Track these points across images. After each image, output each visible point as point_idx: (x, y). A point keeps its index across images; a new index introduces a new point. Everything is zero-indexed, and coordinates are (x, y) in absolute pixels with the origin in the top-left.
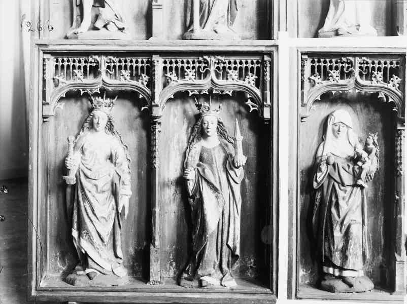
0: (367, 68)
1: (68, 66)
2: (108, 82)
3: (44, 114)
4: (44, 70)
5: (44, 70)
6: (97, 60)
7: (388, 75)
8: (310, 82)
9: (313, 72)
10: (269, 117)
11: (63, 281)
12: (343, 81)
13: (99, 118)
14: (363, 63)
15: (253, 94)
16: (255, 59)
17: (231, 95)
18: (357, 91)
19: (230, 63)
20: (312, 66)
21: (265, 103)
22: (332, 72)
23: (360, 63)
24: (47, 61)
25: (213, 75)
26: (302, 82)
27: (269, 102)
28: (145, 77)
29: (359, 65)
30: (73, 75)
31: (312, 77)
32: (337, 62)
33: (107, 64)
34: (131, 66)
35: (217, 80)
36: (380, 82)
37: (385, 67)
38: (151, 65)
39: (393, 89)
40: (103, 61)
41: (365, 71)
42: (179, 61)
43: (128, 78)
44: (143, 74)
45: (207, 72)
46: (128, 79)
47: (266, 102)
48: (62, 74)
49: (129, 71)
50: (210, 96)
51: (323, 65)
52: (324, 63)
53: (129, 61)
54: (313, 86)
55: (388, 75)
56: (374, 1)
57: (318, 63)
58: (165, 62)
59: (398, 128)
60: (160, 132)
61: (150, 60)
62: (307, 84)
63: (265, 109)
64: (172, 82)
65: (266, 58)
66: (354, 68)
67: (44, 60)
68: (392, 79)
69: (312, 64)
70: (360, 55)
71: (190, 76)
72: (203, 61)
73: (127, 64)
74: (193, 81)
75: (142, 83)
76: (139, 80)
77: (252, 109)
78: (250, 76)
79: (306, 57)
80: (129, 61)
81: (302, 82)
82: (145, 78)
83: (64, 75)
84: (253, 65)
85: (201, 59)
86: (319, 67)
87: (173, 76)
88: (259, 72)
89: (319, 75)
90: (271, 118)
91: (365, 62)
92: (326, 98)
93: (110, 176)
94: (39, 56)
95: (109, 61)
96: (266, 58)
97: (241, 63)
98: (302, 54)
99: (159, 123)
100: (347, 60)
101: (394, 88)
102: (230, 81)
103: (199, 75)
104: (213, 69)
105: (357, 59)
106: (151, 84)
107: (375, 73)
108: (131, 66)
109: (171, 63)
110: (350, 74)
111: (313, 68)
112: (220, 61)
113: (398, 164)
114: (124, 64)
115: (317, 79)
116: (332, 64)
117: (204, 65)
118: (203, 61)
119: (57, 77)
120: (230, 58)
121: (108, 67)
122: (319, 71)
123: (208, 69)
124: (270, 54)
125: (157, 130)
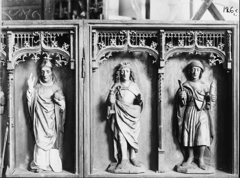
0: (135, 37)
1: (20, 39)
6: (124, 33)
7: (218, 42)
9: (100, 41)
10: (73, 68)
11: (175, 171)
12: (188, 46)
14: (132, 35)
17: (112, 55)
19: (181, 35)
23: (198, 36)
25: (129, 43)
26: (93, 47)
31: (100, 43)
33: (44, 37)
35: (198, 46)
36: (211, 46)
37: (205, 38)
38: (159, 35)
40: (128, 34)
41: (134, 40)
45: (125, 42)
46: (211, 45)
47: (229, 59)
50: (195, 56)
51: (106, 36)
52: (205, 36)
53: (22, 36)
54: (100, 49)
55: (218, 42)
56: (204, 1)
57: (145, 36)
58: (16, 36)
61: (6, 34)
62: (96, 47)
63: (71, 63)
64: (170, 49)
65: (229, 32)
67: (93, 33)
68: (219, 44)
69: (198, 37)
71: (113, 43)
72: (190, 34)
73: (28, 37)
74: (115, 46)
78: (221, 44)
79: (94, 31)
80: (22, 36)
81: (93, 47)
85: (121, 32)
86: (103, 38)
87: (103, 44)
88: (225, 40)
89: (104, 42)
90: (74, 69)
91: (133, 34)
92: (116, 55)
93: (52, 118)
95: (132, 34)
96: (229, 32)
98: (93, 29)
99: (163, 74)
100: (191, 34)
102: (53, 48)
104: (129, 38)
105: (129, 31)
106: (159, 48)
107: (112, 40)
109: (212, 35)
111: (100, 38)
113: (8, 90)
114: (26, 37)
115: (170, 45)
117: (123, 36)
118: (190, 34)
120: (167, 32)
121: (45, 39)
123: (126, 39)
124: (73, 29)
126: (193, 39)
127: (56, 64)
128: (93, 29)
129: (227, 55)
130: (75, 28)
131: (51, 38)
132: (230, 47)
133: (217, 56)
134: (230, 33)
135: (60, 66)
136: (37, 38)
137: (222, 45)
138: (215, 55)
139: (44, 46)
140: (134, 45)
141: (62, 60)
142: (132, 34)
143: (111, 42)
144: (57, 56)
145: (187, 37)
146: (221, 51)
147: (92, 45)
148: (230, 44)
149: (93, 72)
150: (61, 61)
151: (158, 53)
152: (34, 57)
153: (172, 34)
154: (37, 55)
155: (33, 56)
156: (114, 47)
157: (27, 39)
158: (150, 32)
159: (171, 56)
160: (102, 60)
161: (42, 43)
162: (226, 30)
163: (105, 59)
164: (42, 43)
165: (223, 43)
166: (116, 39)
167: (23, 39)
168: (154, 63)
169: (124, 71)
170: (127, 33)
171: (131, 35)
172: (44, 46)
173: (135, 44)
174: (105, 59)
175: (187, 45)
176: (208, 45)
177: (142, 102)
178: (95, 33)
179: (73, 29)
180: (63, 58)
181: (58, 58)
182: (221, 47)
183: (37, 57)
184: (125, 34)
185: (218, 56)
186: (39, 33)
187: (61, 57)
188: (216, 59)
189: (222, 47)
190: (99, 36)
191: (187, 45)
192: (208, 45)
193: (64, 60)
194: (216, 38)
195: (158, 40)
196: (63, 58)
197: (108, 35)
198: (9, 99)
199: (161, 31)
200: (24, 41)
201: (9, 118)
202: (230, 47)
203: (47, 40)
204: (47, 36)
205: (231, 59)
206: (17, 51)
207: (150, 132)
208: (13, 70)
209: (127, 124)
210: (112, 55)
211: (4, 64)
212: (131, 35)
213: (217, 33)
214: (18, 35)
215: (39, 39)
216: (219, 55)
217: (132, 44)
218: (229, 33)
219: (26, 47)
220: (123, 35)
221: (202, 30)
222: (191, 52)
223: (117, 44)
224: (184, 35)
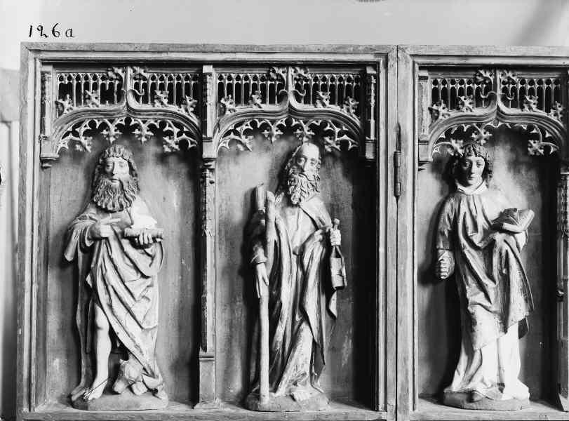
0: (514, 90)
2: (482, 114)
3: (44, 154)
4: (43, 89)
5: (43, 89)
6: (281, 76)
8: (57, 107)
13: (114, 163)
14: (508, 83)
15: (351, 126)
16: (190, 72)
17: (124, 124)
18: (500, 124)
19: (532, 83)
20: (219, 84)
21: (204, 136)
22: (462, 98)
23: (504, 83)
24: (47, 75)
27: (372, 137)
28: (190, 100)
29: (502, 86)
30: (85, 99)
31: (435, 107)
32: (103, 78)
34: (171, 86)
35: (507, 109)
38: (201, 79)
39: (554, 119)
42: (224, 77)
43: (165, 101)
44: (189, 95)
47: (369, 137)
48: (230, 96)
49: (168, 92)
53: (66, 78)
57: (452, 84)
59: (562, 173)
60: (212, 182)
65: (370, 71)
66: (287, 89)
67: (43, 74)
70: (132, 63)
75: (187, 110)
76: (182, 106)
77: (190, 146)
79: (49, 68)
82: (190, 101)
83: (232, 98)
84: (256, 82)
94: (35, 67)
95: (298, 77)
96: (370, 71)
97: (238, 78)
101: (556, 118)
103: (107, 96)
106: (201, 111)
108: (171, 86)
110: (491, 100)
112: (511, 81)
116: (155, 81)
119: (435, 107)
121: (137, 86)
122: (230, 92)
125: (208, 180)
126: (284, 90)
127: (326, 147)
128: (421, 68)
129: (366, 125)
130: (378, 63)
131: (150, 83)
132: (372, 108)
133: (182, 129)
134: (372, 74)
135: (176, 150)
136: (490, 87)
137: (352, 103)
138: (177, 125)
139: (134, 104)
140: (305, 103)
141: (545, 140)
142: (506, 80)
143: (87, 96)
144: (534, 131)
145: (476, 86)
146: (557, 121)
147: (42, 101)
148: (373, 101)
149: (419, 170)
150: (177, 139)
151: (358, 122)
152: (108, 130)
153: (233, 75)
154: (148, 126)
155: (268, 128)
156: (96, 108)
157: (162, 87)
158: (258, 72)
159: (230, 129)
160: (227, 139)
161: (499, 99)
162: (362, 65)
163: (232, 136)
164: (499, 99)
165: (356, 99)
166: (99, 90)
167: (154, 86)
168: (351, 149)
169: (471, 163)
170: (287, 77)
171: (295, 79)
172: (134, 104)
173: (145, 101)
174: (232, 136)
175: (270, 103)
176: (526, 108)
177: (334, 248)
178: (48, 73)
179: (375, 65)
180: (548, 135)
181: (536, 137)
182: (559, 113)
183: (116, 131)
184: (121, 78)
185: (344, 129)
186: (491, 76)
187: (544, 134)
188: (340, 134)
189: (561, 113)
190: (433, 86)
191: (270, 103)
192: (526, 108)
193: (550, 140)
194: (453, 88)
195: (199, 92)
196: (548, 135)
197: (344, 81)
198: (205, 236)
199: (206, 69)
200: (155, 89)
201: (24, 289)
202: (372, 108)
203: (303, 88)
204: (140, 79)
205: (372, 137)
206: (443, 118)
207: (58, 330)
208: (215, 159)
209: (125, 307)
210: (124, 124)
211: (350, 144)
212: (504, 83)
213: (544, 76)
214: (174, 78)
215: (491, 90)
216: (187, 128)
217: (299, 101)
218: (370, 75)
219: (464, 109)
220: (116, 79)
221: (305, 65)
222: (489, 124)
223: (103, 102)
224: (263, 79)
